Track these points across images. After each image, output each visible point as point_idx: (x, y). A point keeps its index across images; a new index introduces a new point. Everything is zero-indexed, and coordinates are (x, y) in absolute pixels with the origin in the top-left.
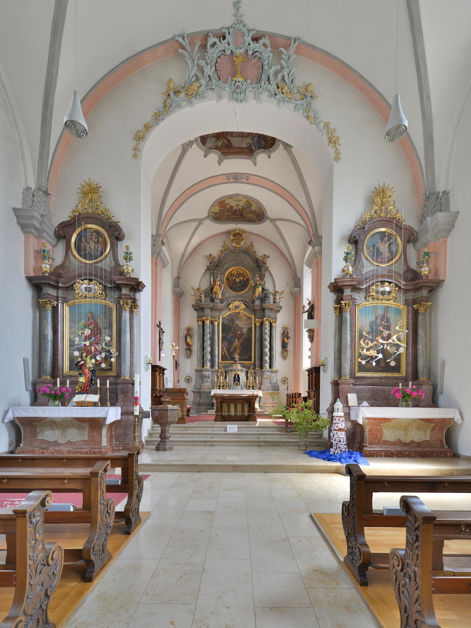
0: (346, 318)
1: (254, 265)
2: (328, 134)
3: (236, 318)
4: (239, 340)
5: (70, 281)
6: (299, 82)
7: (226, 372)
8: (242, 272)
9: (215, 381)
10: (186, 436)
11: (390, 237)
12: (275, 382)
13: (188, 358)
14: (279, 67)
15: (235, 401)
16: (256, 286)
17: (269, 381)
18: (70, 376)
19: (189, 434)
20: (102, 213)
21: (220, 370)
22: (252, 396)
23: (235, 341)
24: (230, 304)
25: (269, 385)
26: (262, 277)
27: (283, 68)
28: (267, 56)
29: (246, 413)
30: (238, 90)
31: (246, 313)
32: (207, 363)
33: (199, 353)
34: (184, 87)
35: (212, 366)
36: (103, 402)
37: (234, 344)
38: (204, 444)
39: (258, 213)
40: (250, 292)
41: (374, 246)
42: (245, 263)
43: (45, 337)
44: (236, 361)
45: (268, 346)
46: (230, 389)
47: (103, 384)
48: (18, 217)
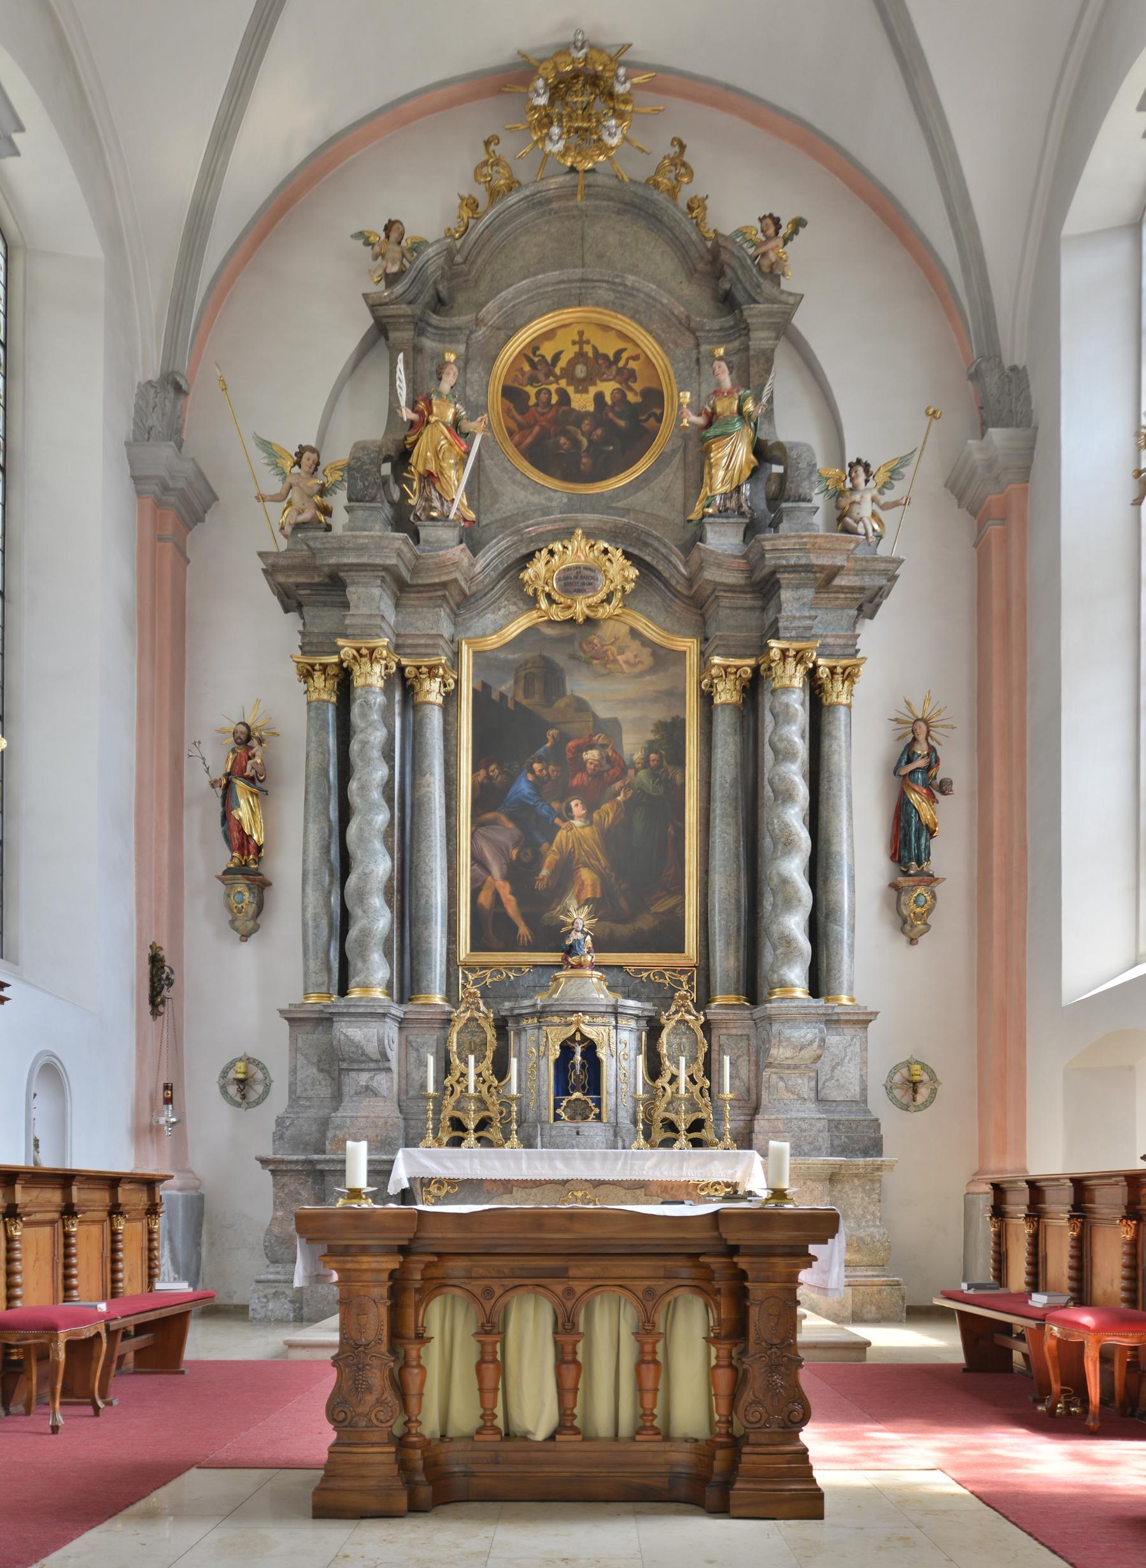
3: (573, 657)
4: (591, 807)
7: (501, 1027)
8: (609, 347)
9: (424, 1086)
12: (854, 1091)
13: (245, 937)
15: (560, 1274)
17: (804, 1086)
21: (462, 1016)
22: (759, 1219)
23: (569, 815)
24: (530, 556)
25: (810, 1111)
31: (651, 631)
32: (364, 959)
33: (313, 897)
37: (561, 835)
40: (672, 480)
42: (630, 279)
44: (570, 950)
46: (528, 1143)
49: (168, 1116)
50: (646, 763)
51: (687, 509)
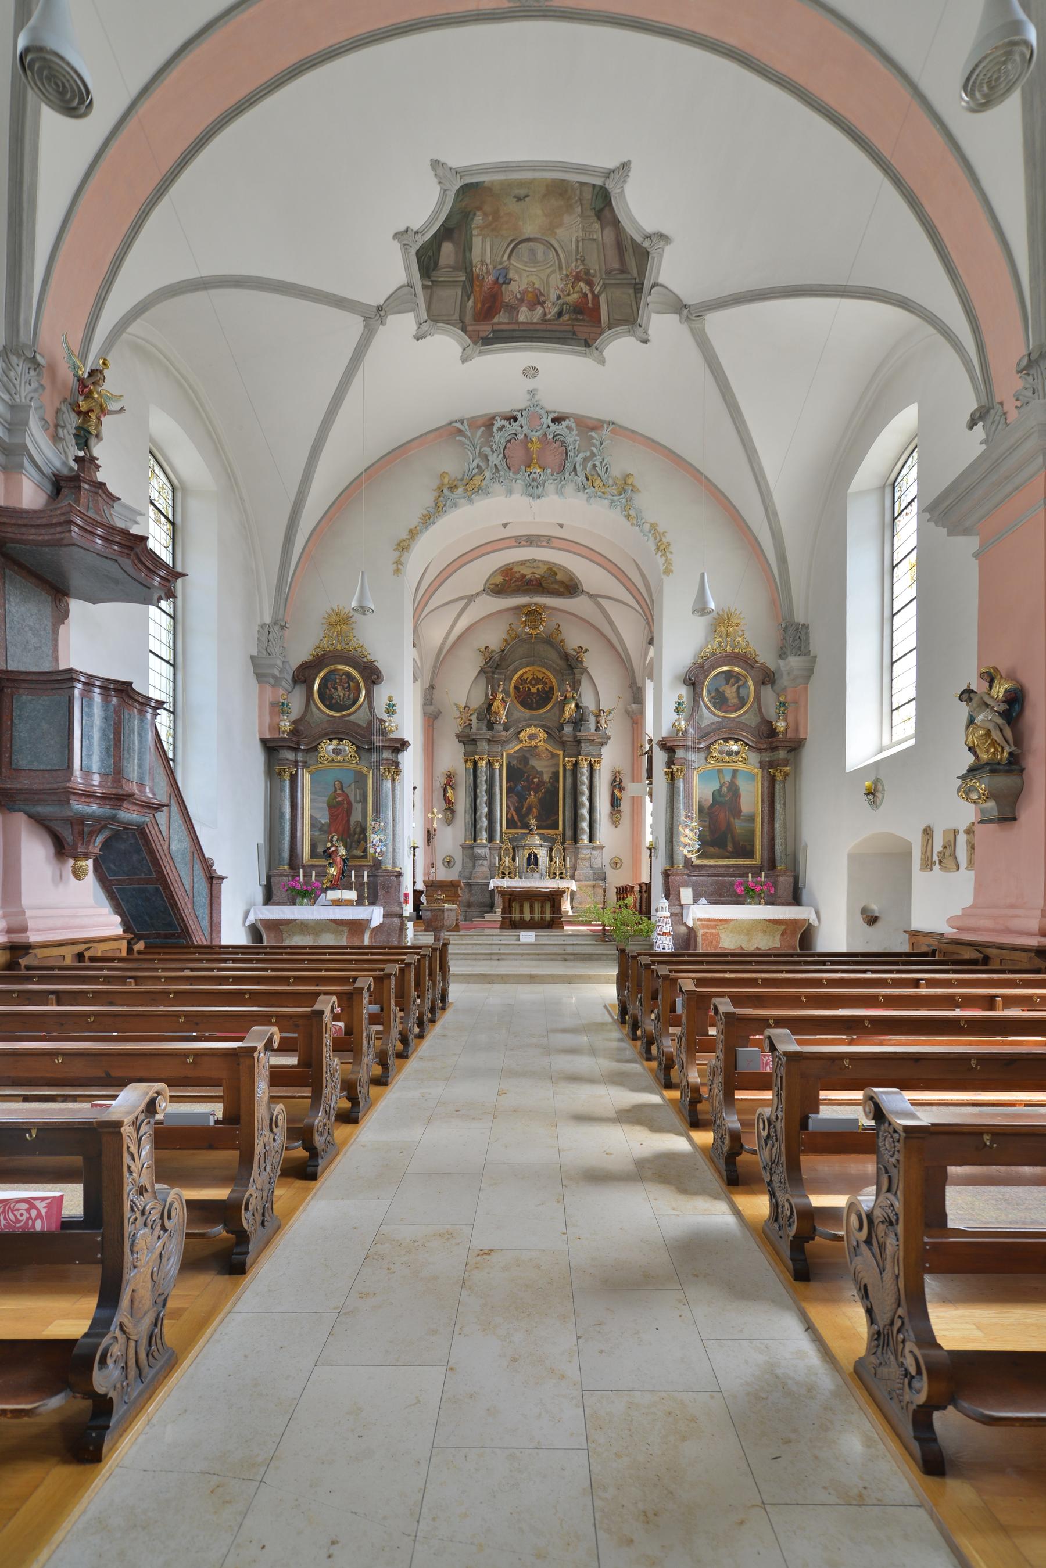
0: (679, 788)
1: (562, 663)
2: (655, 538)
4: (536, 793)
5: (315, 740)
6: (616, 472)
7: (514, 849)
9: (495, 864)
10: (463, 947)
11: (737, 677)
14: (588, 454)
16: (566, 700)
17: (587, 864)
18: (313, 866)
19: (468, 944)
20: (355, 649)
23: (530, 795)
24: (520, 732)
25: (589, 870)
26: (576, 686)
27: (593, 455)
28: (572, 439)
29: (548, 916)
30: (535, 484)
31: (550, 749)
34: (462, 480)
35: (491, 839)
36: (360, 902)
38: (488, 957)
39: (568, 583)
40: (556, 710)
41: (717, 690)
43: (282, 815)
44: (531, 830)
45: (587, 803)
47: (359, 876)
48: (255, 666)
49: (433, 870)
50: (549, 782)
51: (560, 720)
